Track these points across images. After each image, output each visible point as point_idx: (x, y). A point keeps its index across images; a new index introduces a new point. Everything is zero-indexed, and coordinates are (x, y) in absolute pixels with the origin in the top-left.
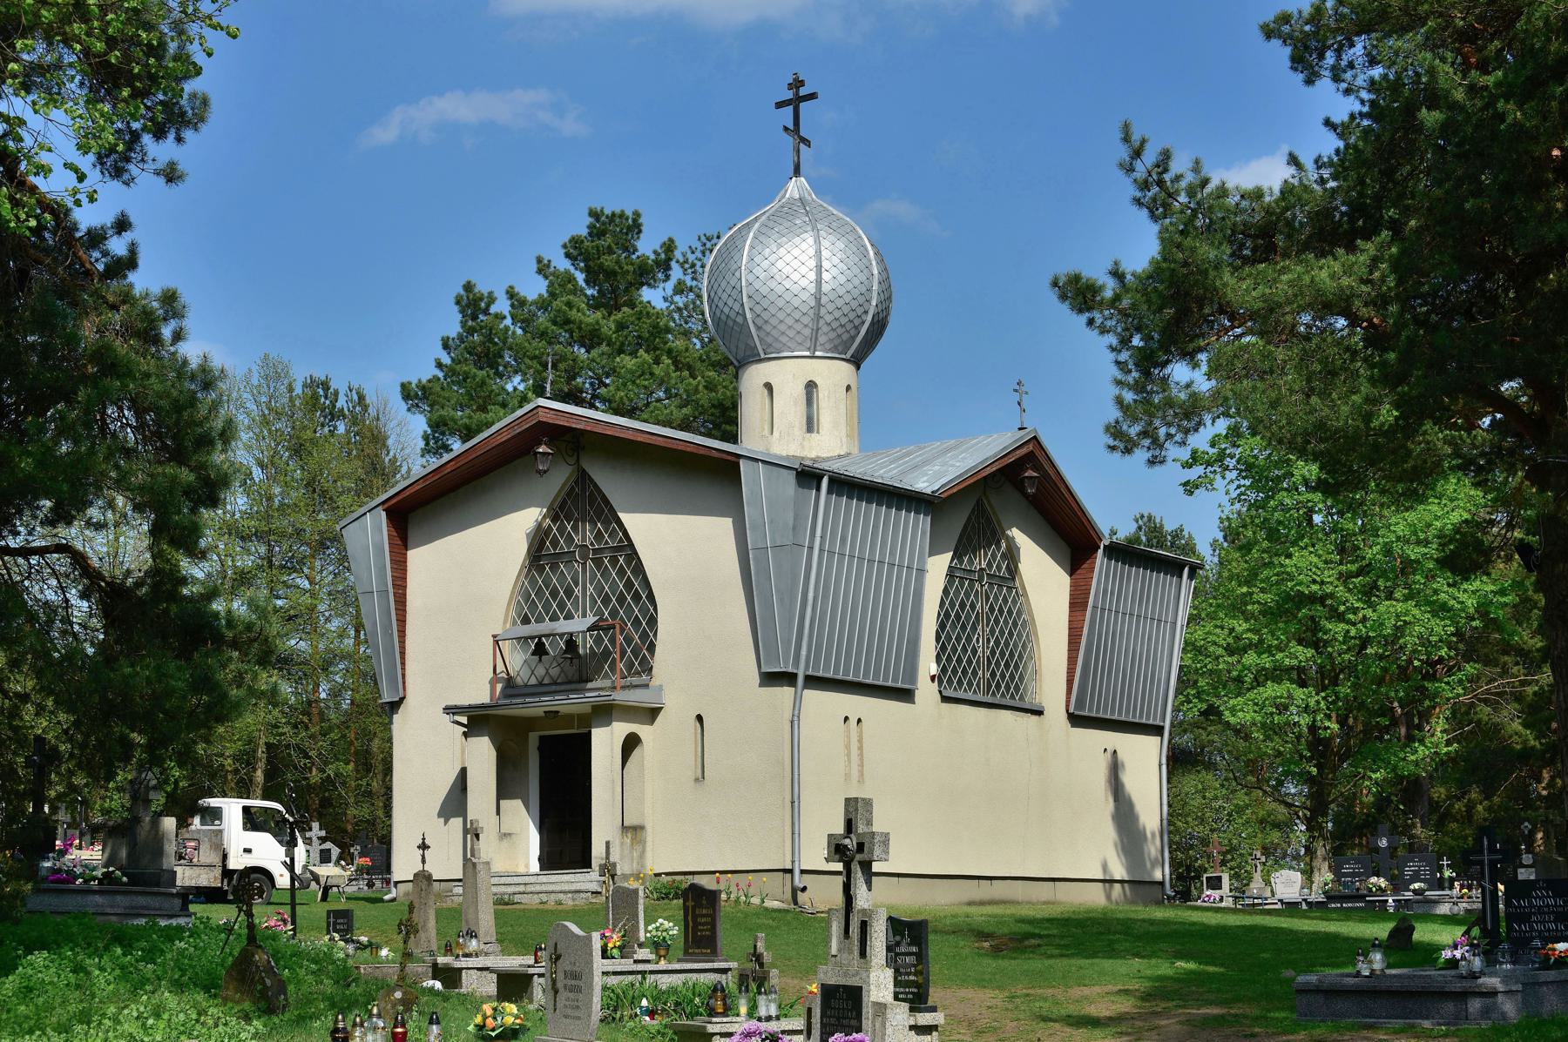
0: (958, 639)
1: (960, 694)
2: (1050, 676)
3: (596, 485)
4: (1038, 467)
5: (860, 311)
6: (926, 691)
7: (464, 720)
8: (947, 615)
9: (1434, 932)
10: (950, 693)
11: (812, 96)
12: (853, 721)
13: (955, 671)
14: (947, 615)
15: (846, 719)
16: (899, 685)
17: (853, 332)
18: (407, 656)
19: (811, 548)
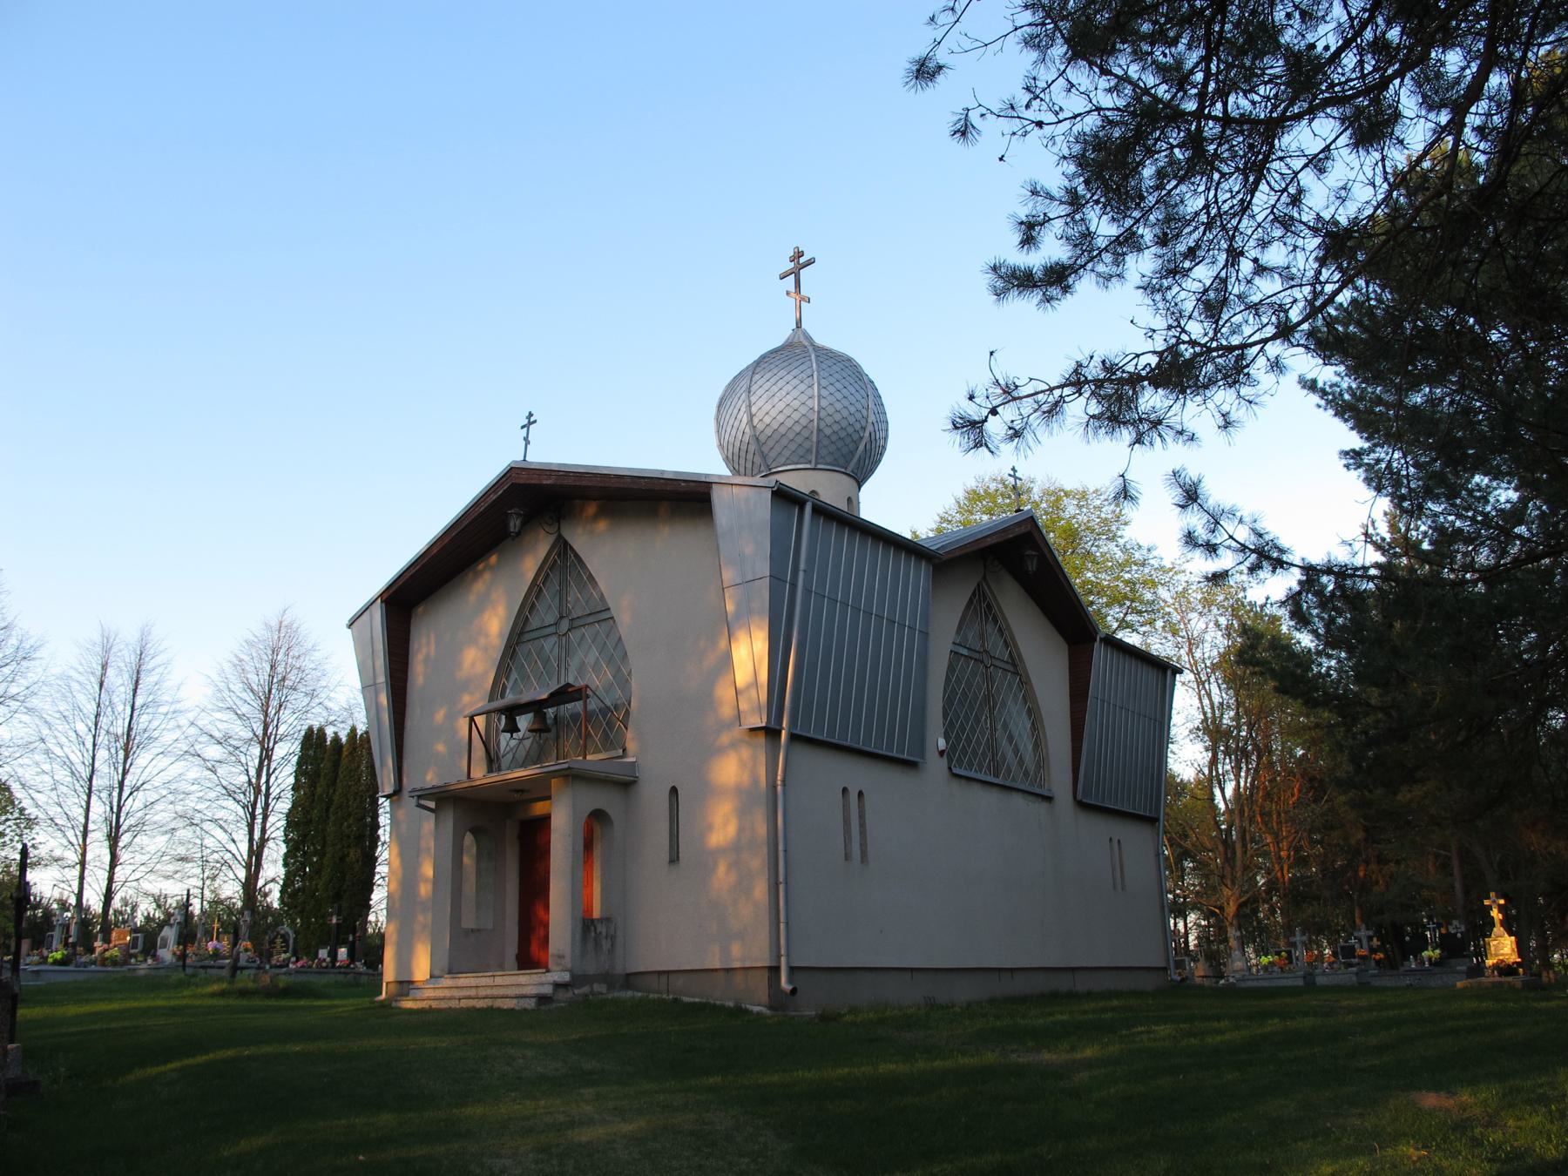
0: (967, 718)
1: (972, 774)
2: (1060, 780)
3: (577, 555)
4: (1036, 547)
5: (855, 437)
6: (936, 767)
7: (432, 805)
8: (954, 691)
9: (1073, 1049)
10: (956, 771)
11: (811, 262)
12: (853, 796)
13: (964, 751)
14: (954, 691)
15: (845, 790)
16: (905, 756)
17: (852, 446)
18: (406, 756)
19: (794, 585)
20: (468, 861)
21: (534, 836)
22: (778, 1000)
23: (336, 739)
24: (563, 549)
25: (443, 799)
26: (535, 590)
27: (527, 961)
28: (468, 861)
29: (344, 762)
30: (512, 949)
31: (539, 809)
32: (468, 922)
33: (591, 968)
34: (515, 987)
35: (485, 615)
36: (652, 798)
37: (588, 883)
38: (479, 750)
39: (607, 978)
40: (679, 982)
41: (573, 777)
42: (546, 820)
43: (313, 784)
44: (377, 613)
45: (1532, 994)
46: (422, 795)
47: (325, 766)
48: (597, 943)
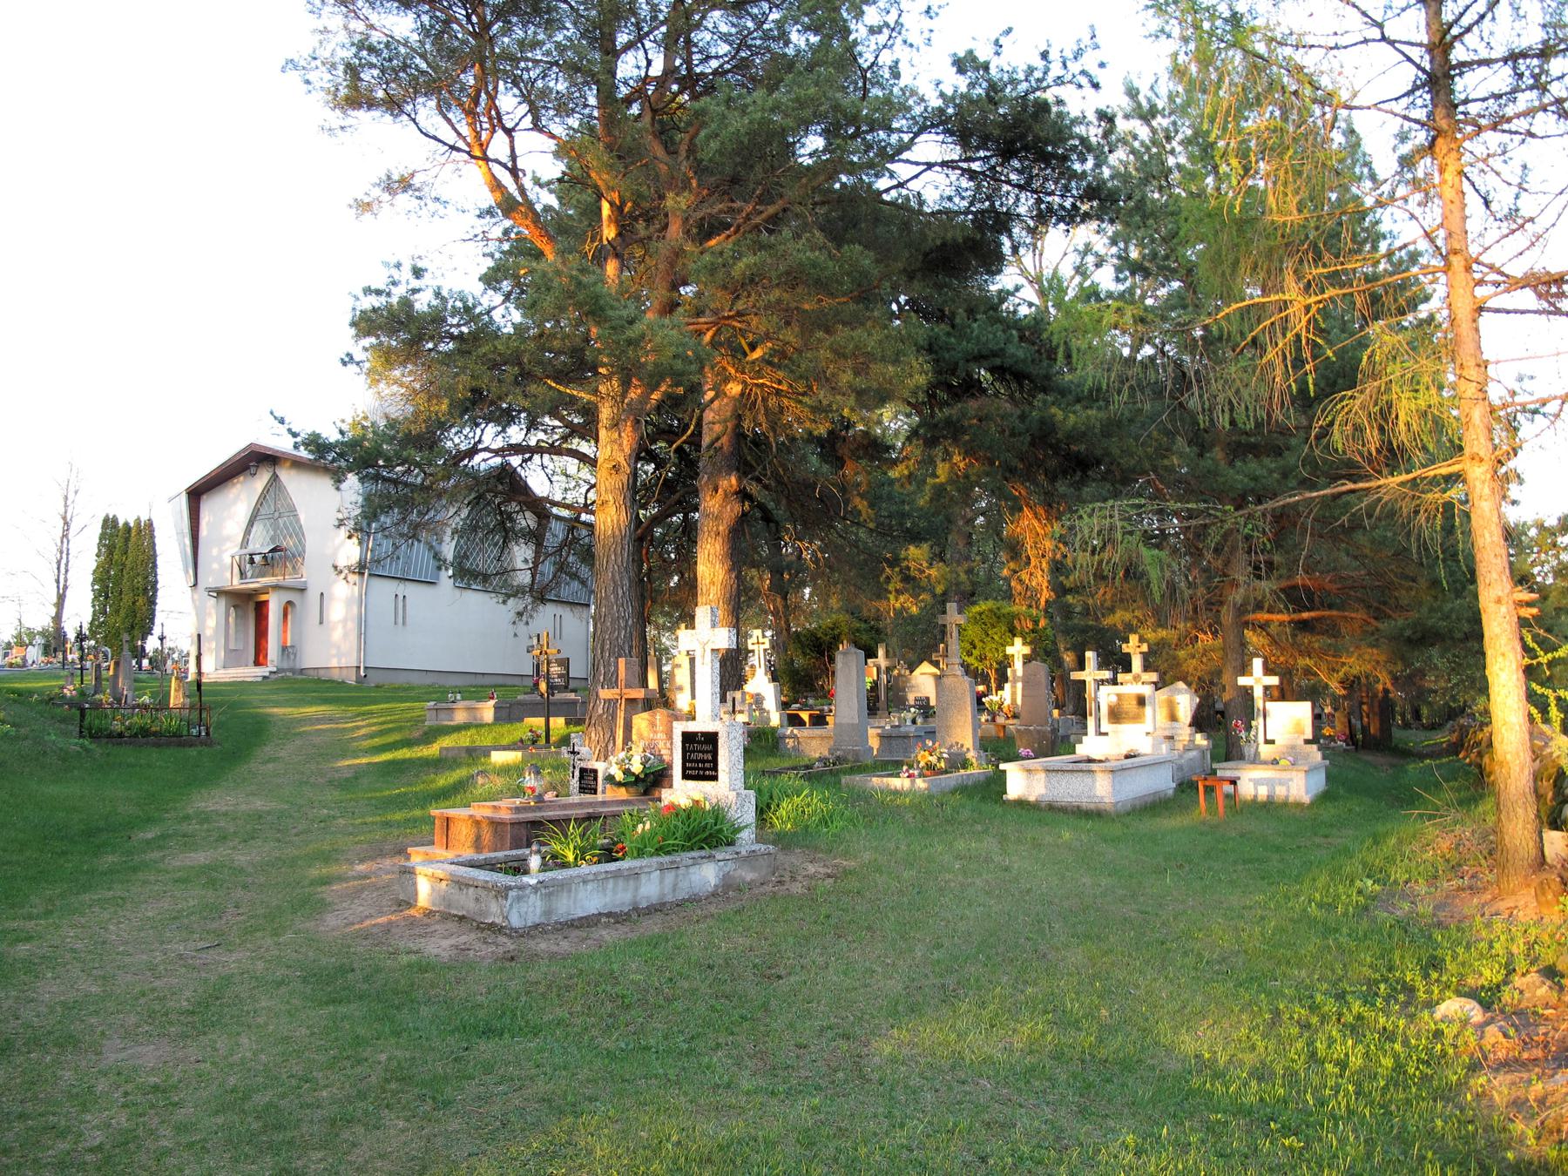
20: (231, 620)
21: (261, 610)
22: (359, 680)
23: (126, 524)
24: (275, 477)
25: (220, 593)
26: (263, 497)
27: (257, 663)
28: (231, 620)
29: (133, 539)
30: (252, 658)
31: (263, 598)
32: (232, 646)
33: (285, 666)
34: (251, 673)
35: (238, 502)
36: (313, 595)
37: (285, 632)
38: (236, 569)
39: (293, 670)
40: (322, 672)
41: (277, 587)
42: (266, 603)
43: (110, 552)
44: (184, 498)
45: (236, 698)
46: (210, 590)
47: (119, 542)
48: (502, 969)
